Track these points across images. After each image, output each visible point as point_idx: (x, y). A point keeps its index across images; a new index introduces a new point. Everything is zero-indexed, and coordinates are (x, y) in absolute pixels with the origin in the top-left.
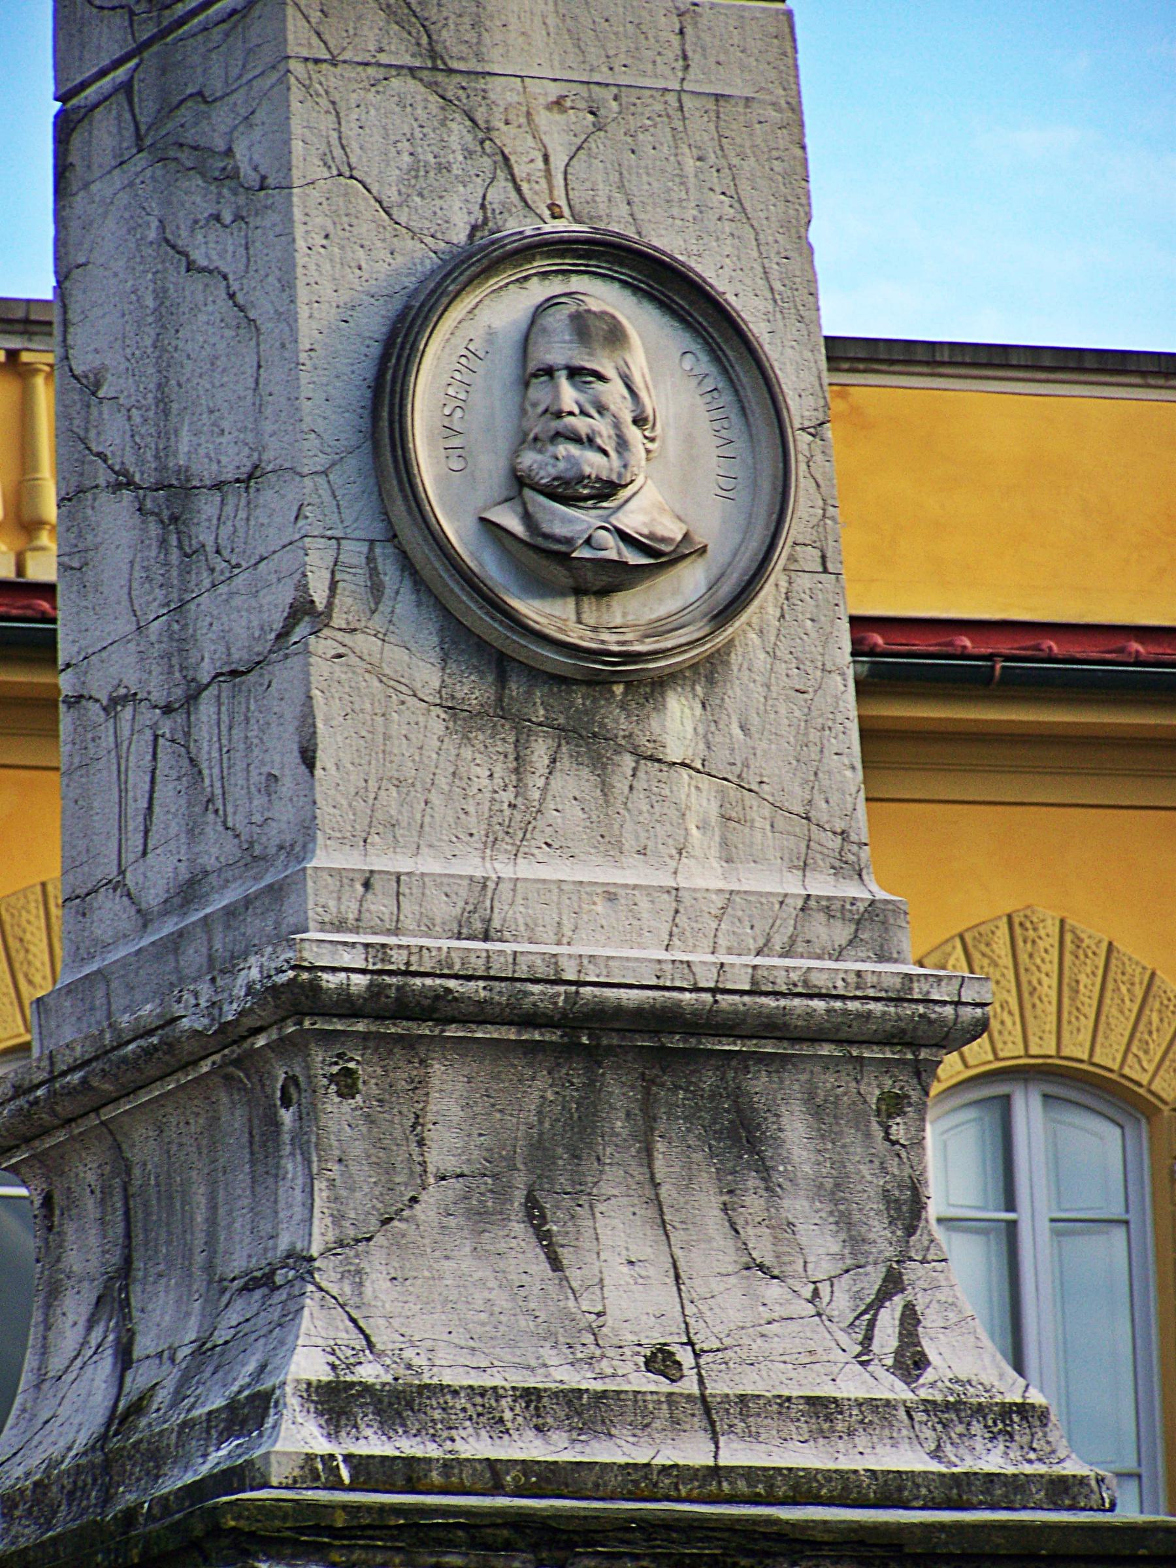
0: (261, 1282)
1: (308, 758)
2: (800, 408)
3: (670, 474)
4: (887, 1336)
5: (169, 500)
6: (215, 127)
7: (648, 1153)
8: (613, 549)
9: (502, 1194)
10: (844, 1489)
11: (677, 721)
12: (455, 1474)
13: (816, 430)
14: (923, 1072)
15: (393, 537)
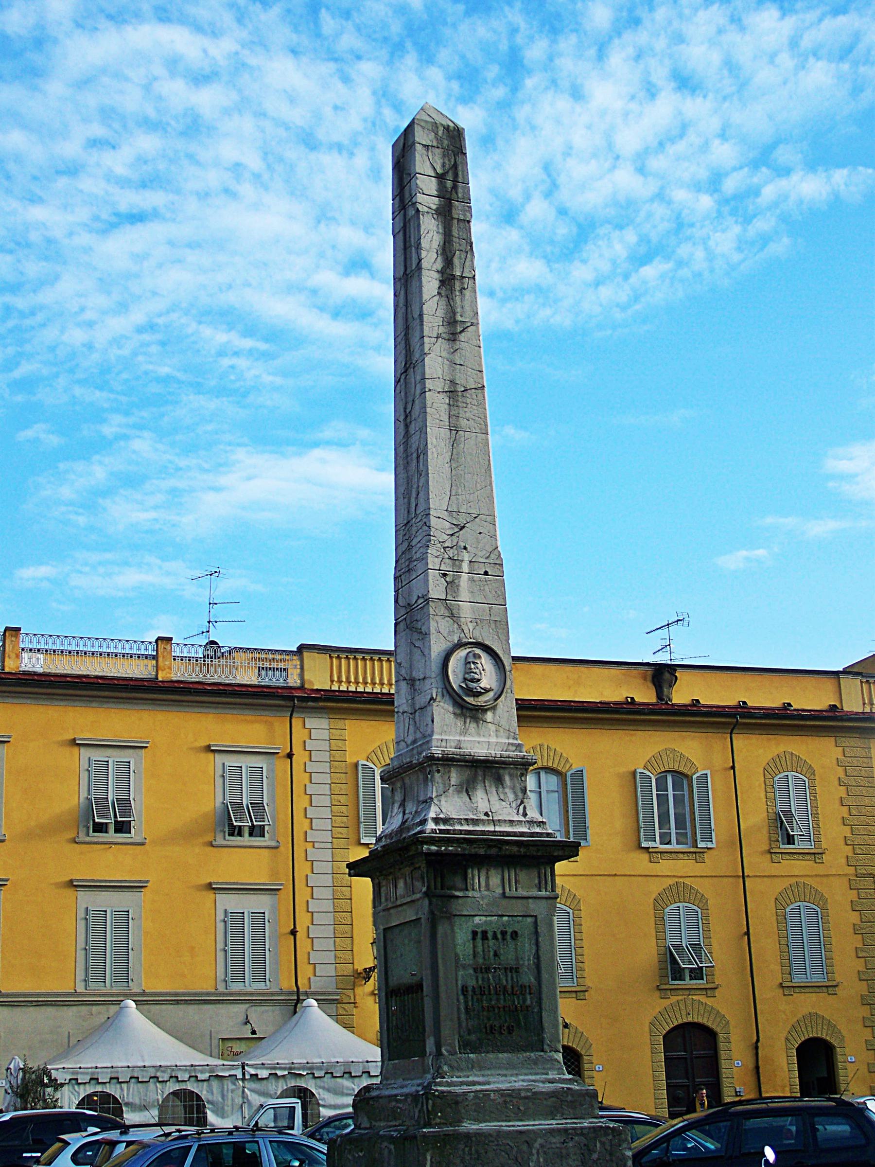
0: (425, 802)
1: (433, 721)
2: (507, 668)
3: (488, 678)
4: (521, 811)
5: (411, 682)
6: (419, 625)
7: (484, 782)
8: (479, 690)
9: (462, 788)
10: (514, 834)
11: (489, 716)
12: (455, 832)
13: (510, 671)
14: (527, 770)
15: (446, 688)
